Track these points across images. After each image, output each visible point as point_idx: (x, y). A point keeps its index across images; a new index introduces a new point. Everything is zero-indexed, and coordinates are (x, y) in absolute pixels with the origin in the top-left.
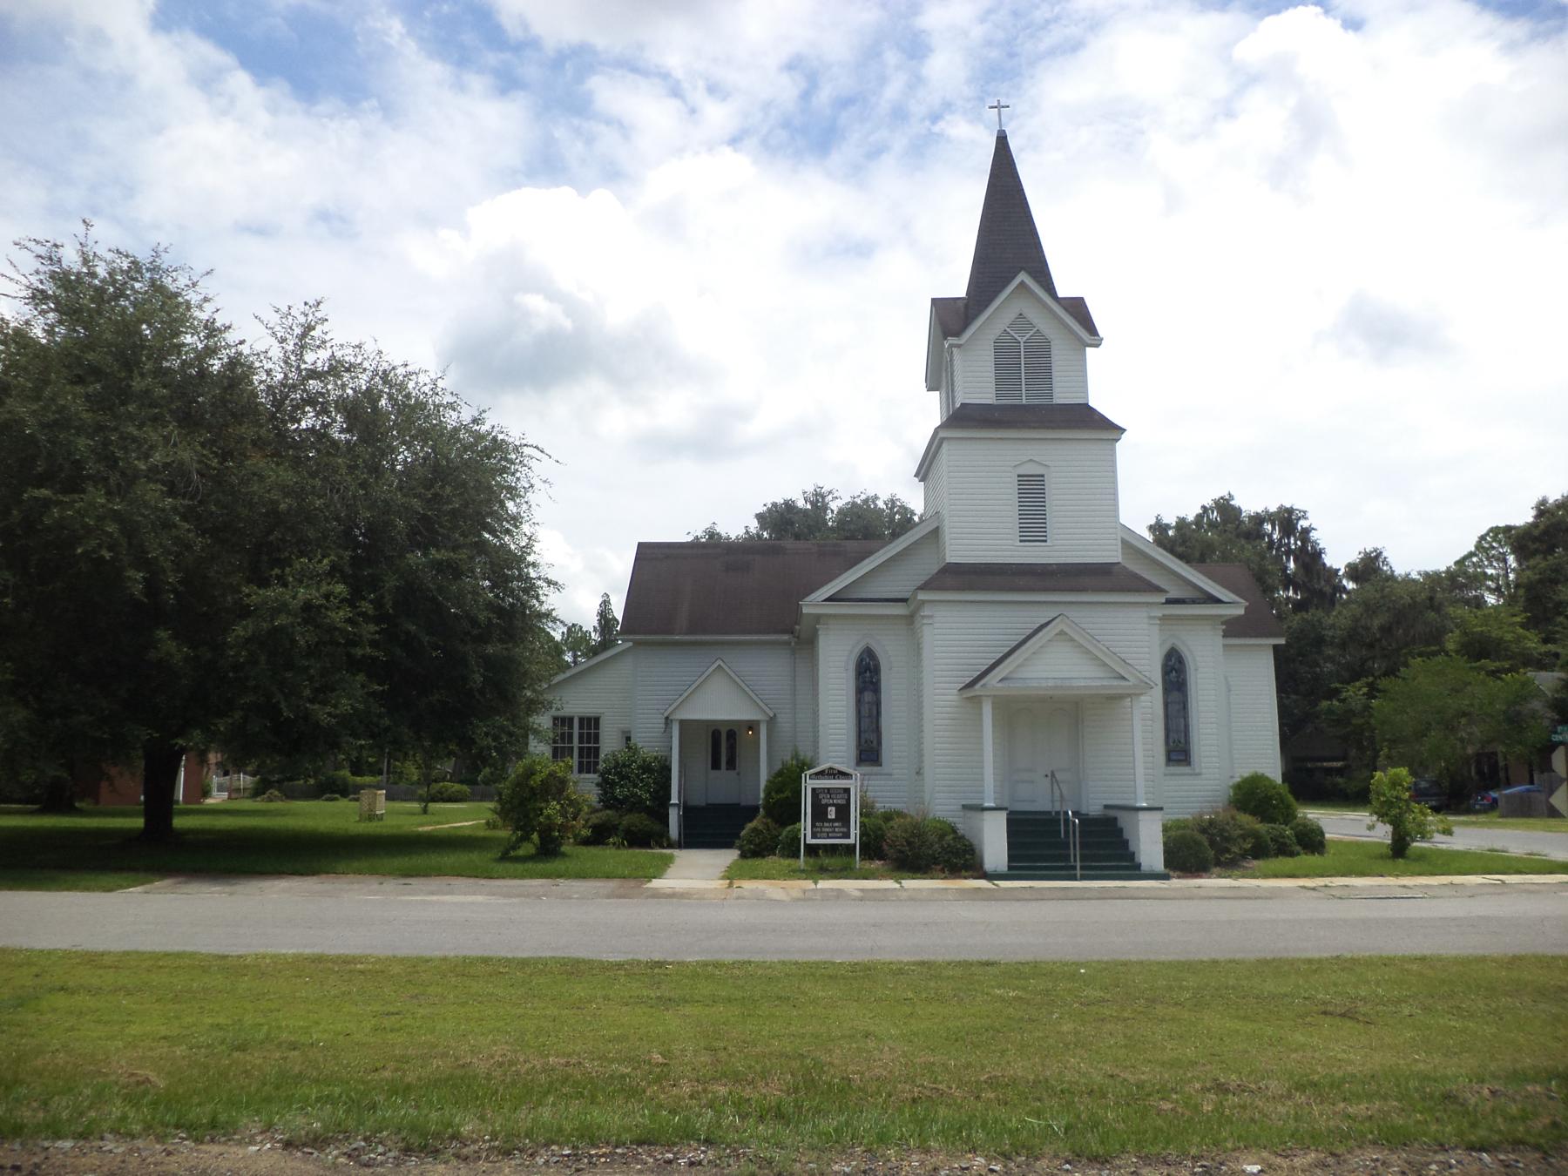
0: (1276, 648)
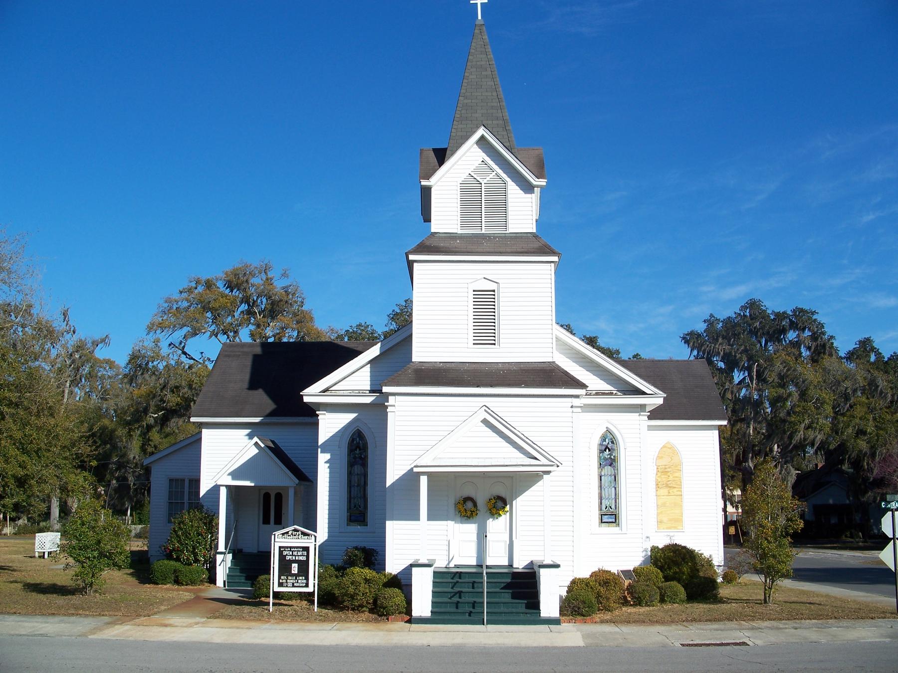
0: (720, 429)
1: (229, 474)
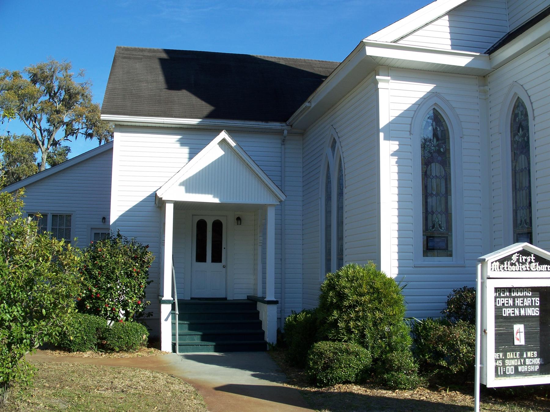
1: (182, 184)
